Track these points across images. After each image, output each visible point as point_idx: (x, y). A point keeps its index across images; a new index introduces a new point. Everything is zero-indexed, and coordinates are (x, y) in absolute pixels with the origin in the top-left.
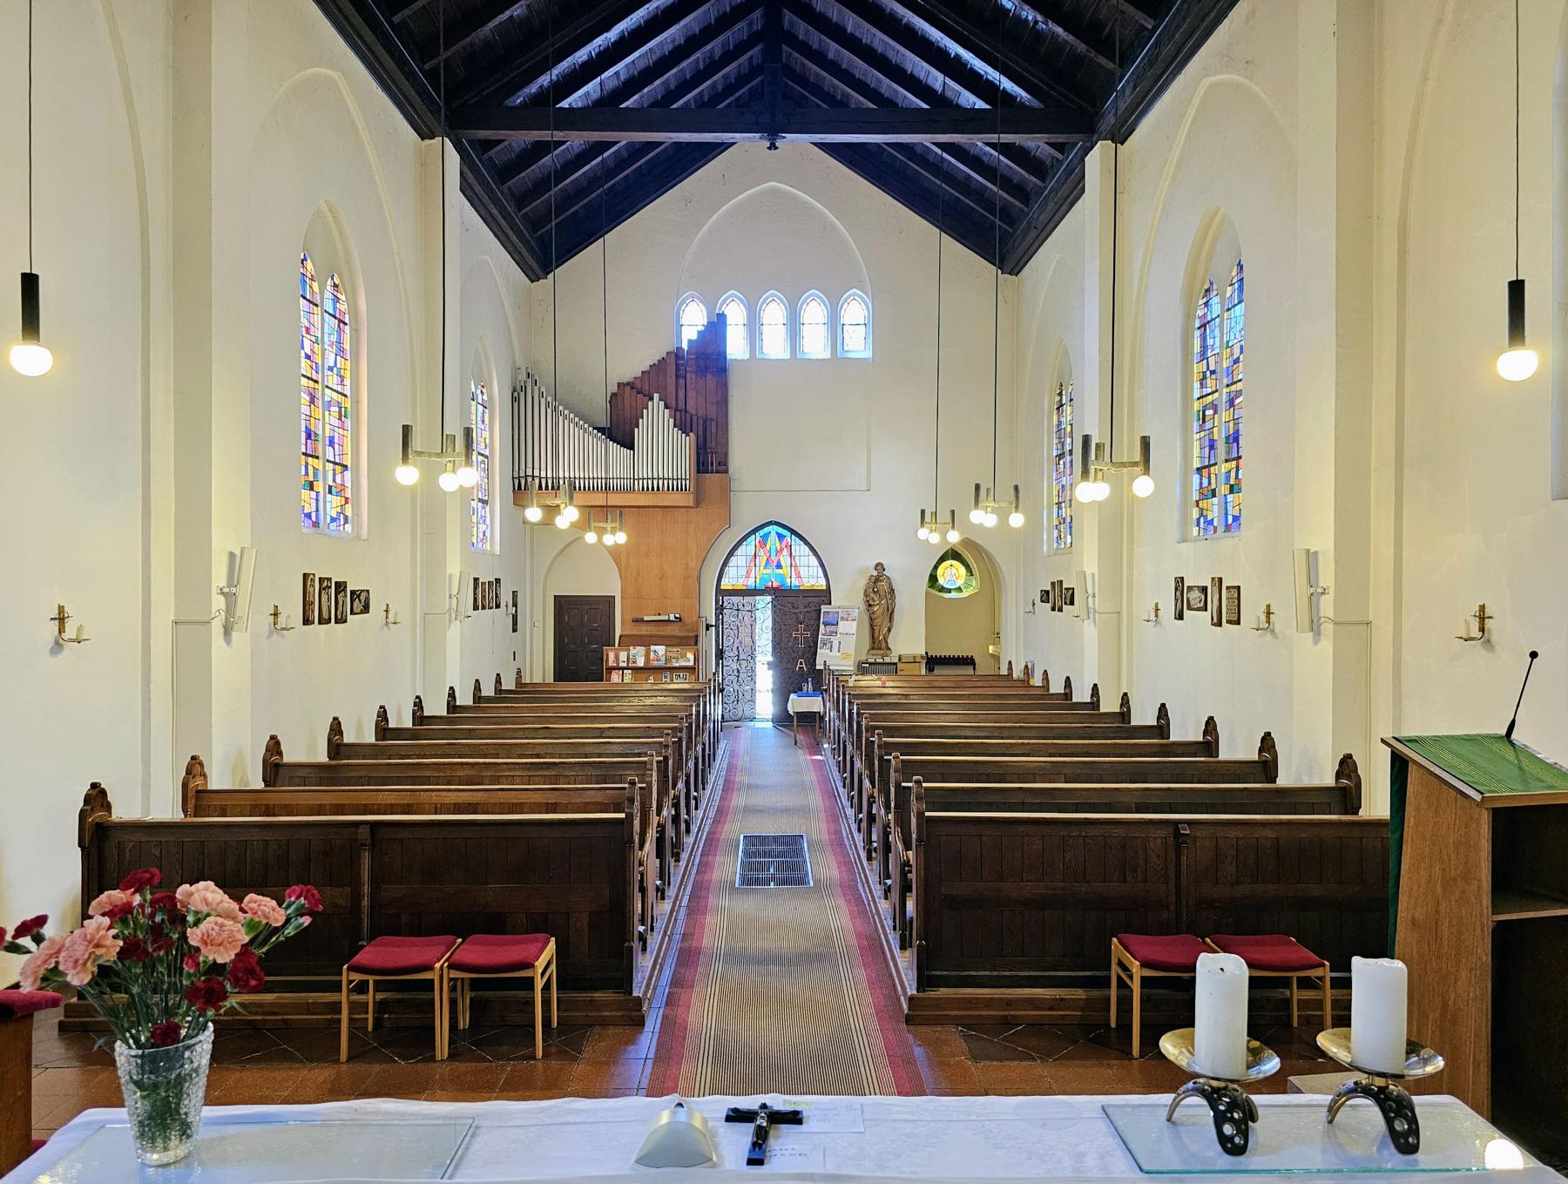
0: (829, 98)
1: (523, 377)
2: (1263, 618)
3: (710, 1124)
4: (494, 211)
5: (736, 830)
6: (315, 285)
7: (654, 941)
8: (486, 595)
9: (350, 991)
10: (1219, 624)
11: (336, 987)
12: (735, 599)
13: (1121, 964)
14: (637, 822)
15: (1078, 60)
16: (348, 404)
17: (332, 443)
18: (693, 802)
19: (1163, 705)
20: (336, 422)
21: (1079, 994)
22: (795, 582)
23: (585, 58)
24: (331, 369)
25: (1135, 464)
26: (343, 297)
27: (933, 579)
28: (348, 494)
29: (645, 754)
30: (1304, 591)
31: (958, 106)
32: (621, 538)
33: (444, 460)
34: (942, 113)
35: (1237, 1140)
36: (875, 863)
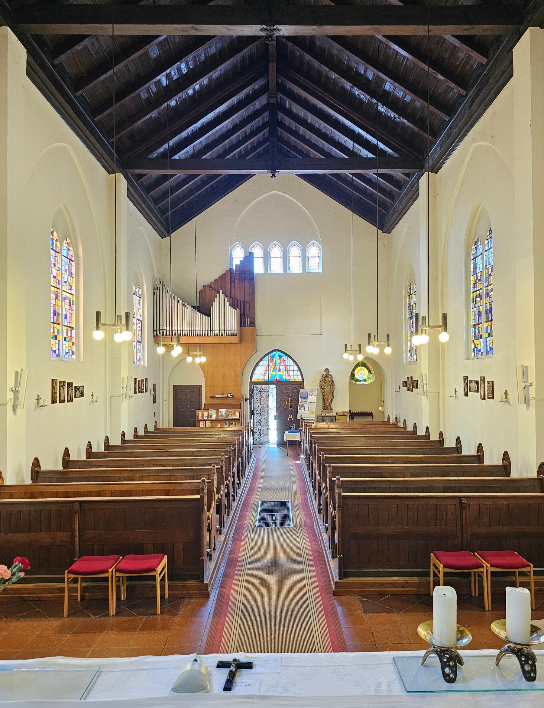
0: (300, 152)
1: (158, 283)
2: (504, 396)
3: (209, 669)
4: (144, 206)
5: (257, 499)
6: (58, 243)
7: (215, 555)
8: (140, 386)
9: (69, 583)
10: (484, 399)
11: (62, 580)
12: (259, 386)
13: (435, 566)
14: (206, 500)
15: (414, 135)
16: (74, 298)
17: (66, 317)
18: (237, 486)
19: (458, 438)
20: (68, 307)
21: (416, 579)
22: (287, 378)
23: (186, 135)
24: (66, 282)
25: (440, 327)
26: (71, 249)
27: (353, 375)
28: (142, 352)
29: (210, 465)
30: (521, 385)
31: (360, 156)
32: (203, 359)
33: (116, 328)
34: (354, 160)
35: (451, 675)
36: (322, 515)
